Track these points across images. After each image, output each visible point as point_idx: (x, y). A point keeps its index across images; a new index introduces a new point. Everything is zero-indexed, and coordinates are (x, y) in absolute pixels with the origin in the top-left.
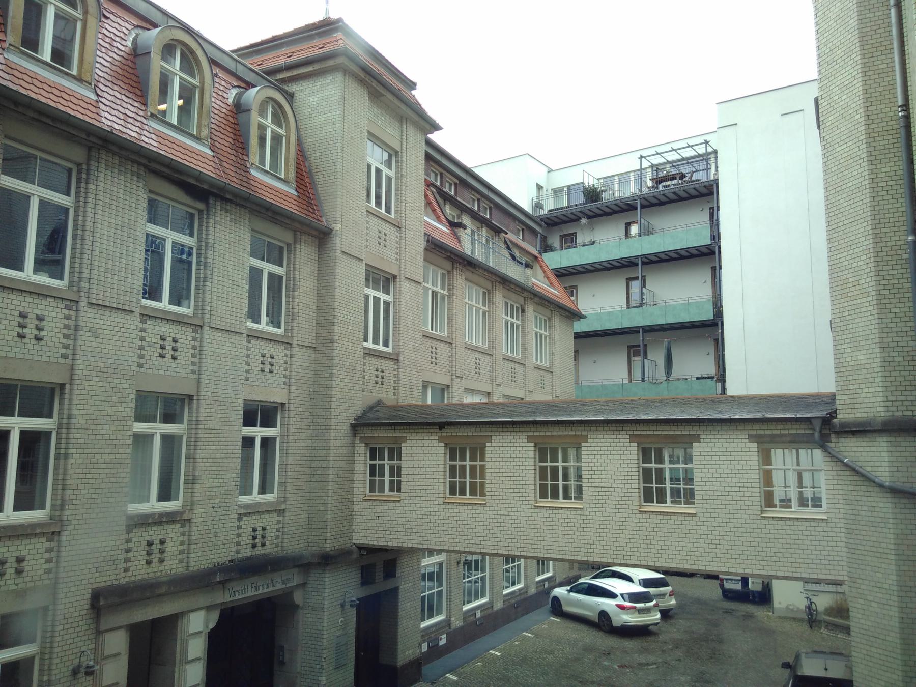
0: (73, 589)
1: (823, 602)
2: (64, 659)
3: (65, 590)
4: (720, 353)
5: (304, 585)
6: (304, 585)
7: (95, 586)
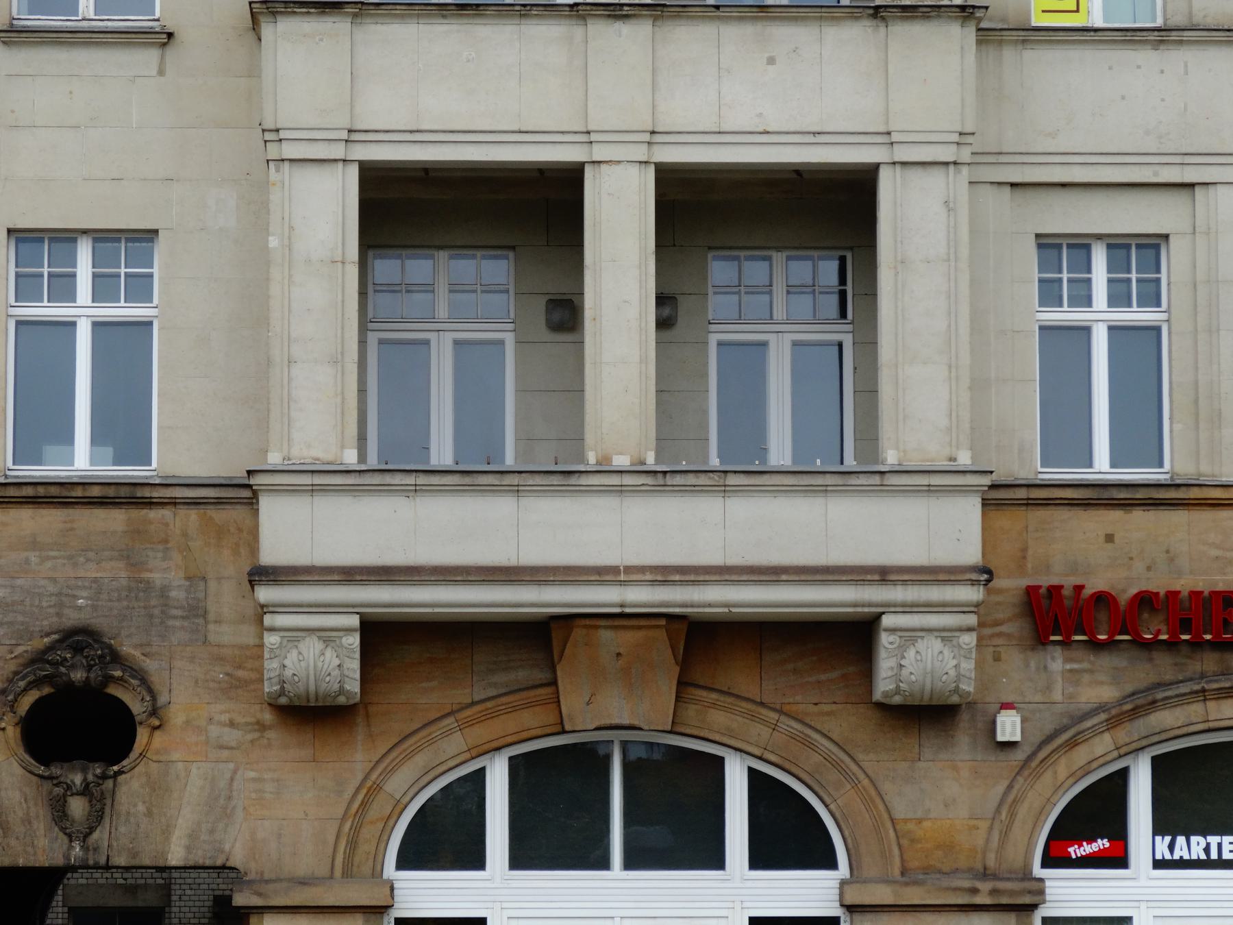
0: (188, 892)
3: (178, 892)
7: (217, 893)
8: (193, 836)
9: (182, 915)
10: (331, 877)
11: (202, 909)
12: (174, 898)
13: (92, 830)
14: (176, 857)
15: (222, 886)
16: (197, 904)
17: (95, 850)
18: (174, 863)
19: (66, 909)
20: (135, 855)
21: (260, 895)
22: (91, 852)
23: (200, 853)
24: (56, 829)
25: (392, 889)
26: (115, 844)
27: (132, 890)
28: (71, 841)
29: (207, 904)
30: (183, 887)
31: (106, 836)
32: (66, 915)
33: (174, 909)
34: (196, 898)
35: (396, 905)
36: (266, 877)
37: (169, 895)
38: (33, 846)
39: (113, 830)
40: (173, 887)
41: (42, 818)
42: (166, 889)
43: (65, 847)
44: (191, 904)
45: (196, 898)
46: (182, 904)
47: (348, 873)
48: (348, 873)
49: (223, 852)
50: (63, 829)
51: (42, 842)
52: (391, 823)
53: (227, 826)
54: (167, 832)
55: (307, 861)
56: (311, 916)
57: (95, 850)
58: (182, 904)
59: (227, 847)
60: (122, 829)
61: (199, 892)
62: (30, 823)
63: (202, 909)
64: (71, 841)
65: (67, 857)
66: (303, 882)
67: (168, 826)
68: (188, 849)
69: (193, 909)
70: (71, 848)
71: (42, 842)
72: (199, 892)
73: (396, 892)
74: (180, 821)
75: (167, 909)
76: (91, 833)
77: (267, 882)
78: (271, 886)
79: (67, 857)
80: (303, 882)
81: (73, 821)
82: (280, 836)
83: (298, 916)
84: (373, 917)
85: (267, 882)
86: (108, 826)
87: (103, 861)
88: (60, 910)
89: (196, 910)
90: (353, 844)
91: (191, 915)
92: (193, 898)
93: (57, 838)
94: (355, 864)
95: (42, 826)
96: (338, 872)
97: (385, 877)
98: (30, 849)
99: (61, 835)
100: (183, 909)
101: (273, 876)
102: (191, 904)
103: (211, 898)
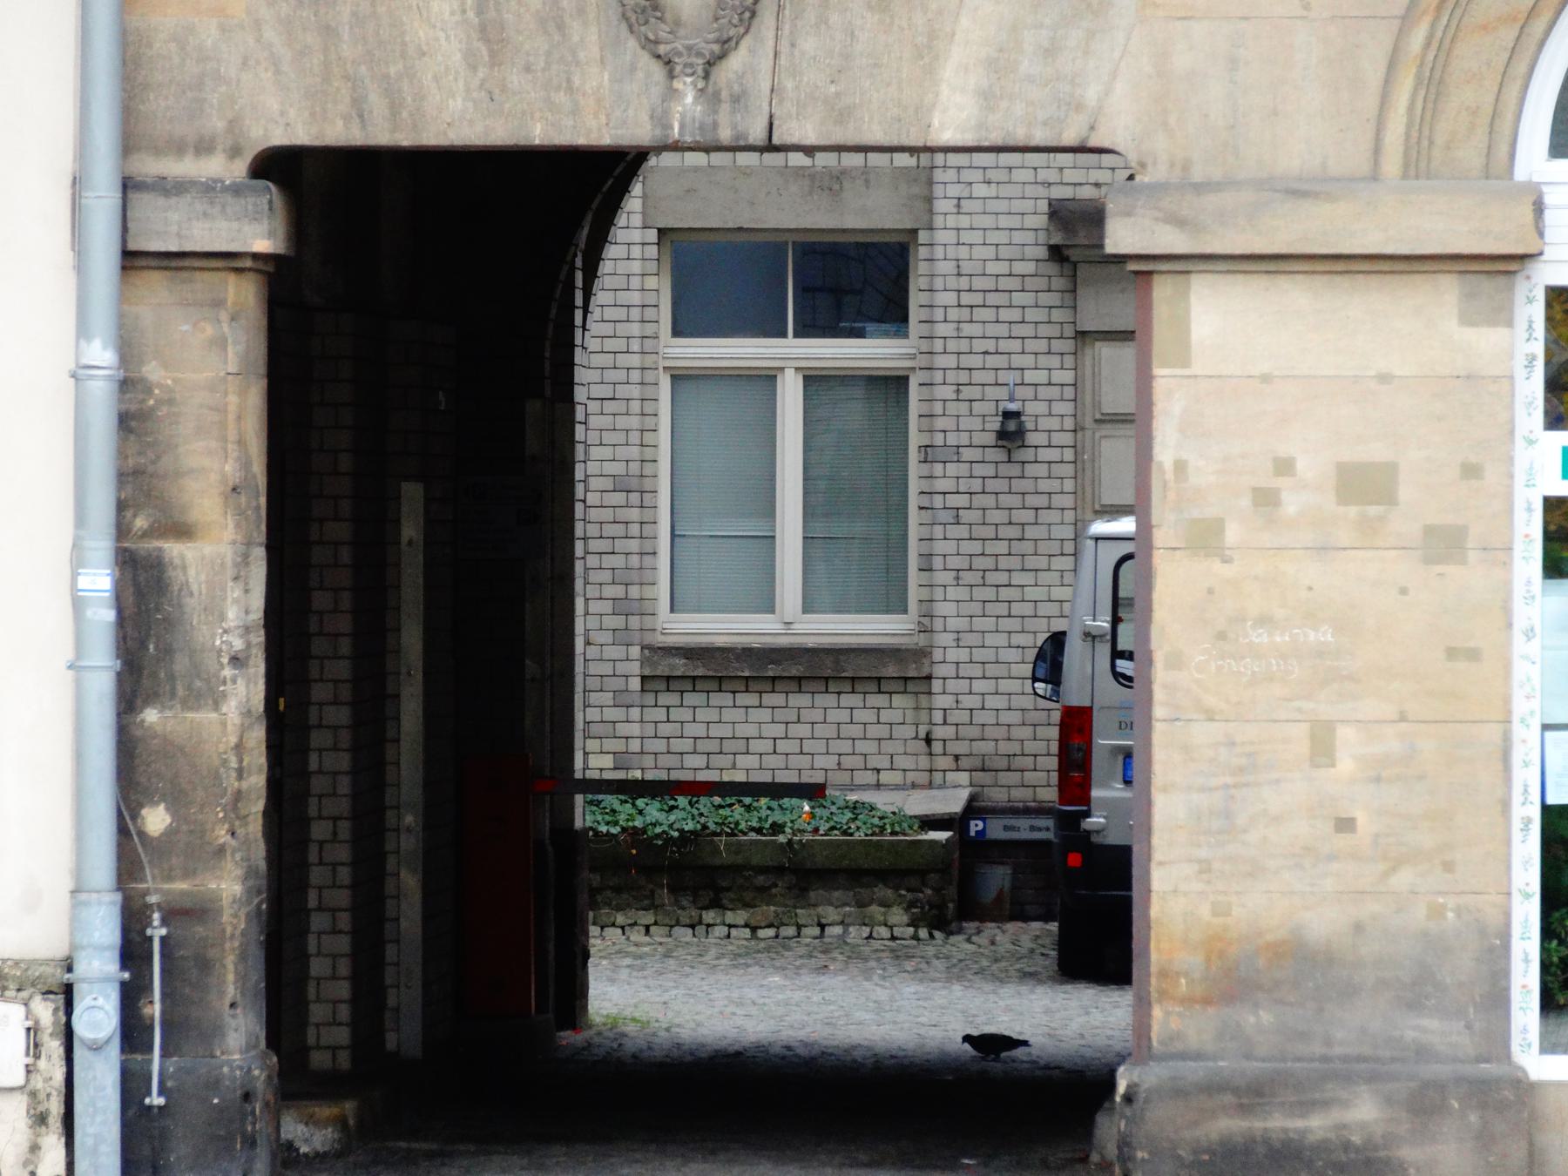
0: (981, 190)
1: (425, 48)
2: (966, 392)
3: (954, 191)
4: (1520, 68)
5: (1186, 975)
6: (1186, 975)
7: (1058, 193)
8: (999, 65)
9: (963, 252)
10: (1375, 176)
11: (1018, 237)
12: (941, 206)
13: (726, 47)
14: (951, 123)
15: (1074, 180)
16: (1004, 221)
17: (736, 99)
18: (947, 137)
19: (652, 235)
20: (843, 115)
21: (1180, 222)
22: (725, 107)
23: (1019, 109)
24: (632, 43)
25: (1539, 208)
26: (789, 84)
27: (833, 183)
28: (671, 76)
29: (1031, 221)
30: (967, 175)
31: (766, 64)
32: (652, 251)
33: (941, 236)
34: (1002, 206)
35: (1547, 250)
36: (1197, 175)
37: (929, 200)
38: (570, 89)
39: (784, 47)
40: (939, 175)
41: (1246, 1064)
42: (923, 186)
43: (656, 91)
44: (988, 221)
45: (1002, 206)
46: (964, 221)
47: (1417, 166)
48: (1417, 166)
49: (1079, 107)
50: (650, 45)
51: (595, 79)
52: (1538, 27)
53: (1091, 34)
54: (929, 52)
55: (1308, 134)
56: (1320, 281)
57: (736, 99)
58: (964, 221)
59: (1091, 94)
60: (808, 44)
61: (1006, 191)
62: (561, 27)
63: (1018, 237)
64: (671, 76)
65: (661, 119)
66: (1299, 191)
67: (932, 35)
68: (988, 98)
69: (993, 237)
70: (671, 94)
71: (595, 79)
72: (1006, 191)
73: (1549, 216)
74: (964, 22)
75: (923, 236)
76: (722, 56)
77: (1200, 188)
78: (1212, 201)
79: (661, 119)
80: (1299, 191)
81: (678, 23)
82: (1233, 63)
83: (1283, 282)
84: (1487, 285)
85: (1200, 188)
86: (771, 34)
87: (757, 134)
88: (636, 236)
89: (1002, 237)
90: (1433, 85)
91: (989, 252)
92: (993, 206)
93: (633, 69)
94: (1440, 140)
95: (593, 37)
96: (1392, 164)
97: (1520, 174)
98: (561, 97)
99: (645, 59)
100: (966, 237)
101: (1217, 174)
102: (988, 221)
103: (1043, 206)
